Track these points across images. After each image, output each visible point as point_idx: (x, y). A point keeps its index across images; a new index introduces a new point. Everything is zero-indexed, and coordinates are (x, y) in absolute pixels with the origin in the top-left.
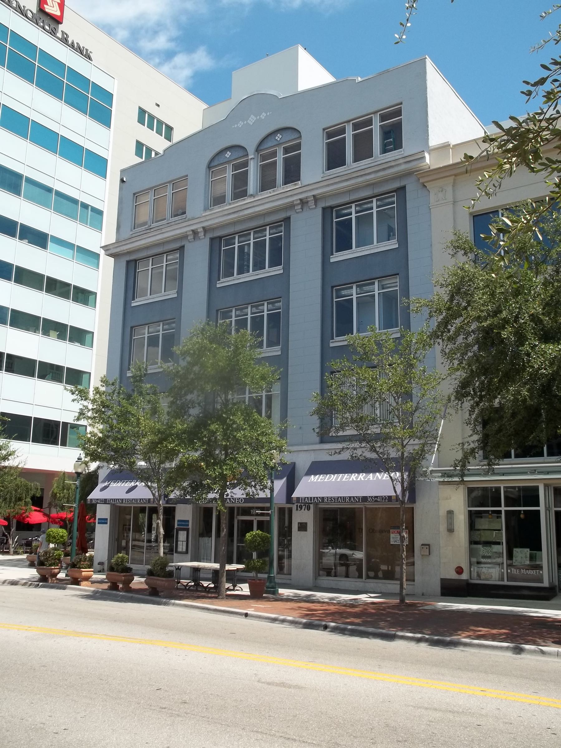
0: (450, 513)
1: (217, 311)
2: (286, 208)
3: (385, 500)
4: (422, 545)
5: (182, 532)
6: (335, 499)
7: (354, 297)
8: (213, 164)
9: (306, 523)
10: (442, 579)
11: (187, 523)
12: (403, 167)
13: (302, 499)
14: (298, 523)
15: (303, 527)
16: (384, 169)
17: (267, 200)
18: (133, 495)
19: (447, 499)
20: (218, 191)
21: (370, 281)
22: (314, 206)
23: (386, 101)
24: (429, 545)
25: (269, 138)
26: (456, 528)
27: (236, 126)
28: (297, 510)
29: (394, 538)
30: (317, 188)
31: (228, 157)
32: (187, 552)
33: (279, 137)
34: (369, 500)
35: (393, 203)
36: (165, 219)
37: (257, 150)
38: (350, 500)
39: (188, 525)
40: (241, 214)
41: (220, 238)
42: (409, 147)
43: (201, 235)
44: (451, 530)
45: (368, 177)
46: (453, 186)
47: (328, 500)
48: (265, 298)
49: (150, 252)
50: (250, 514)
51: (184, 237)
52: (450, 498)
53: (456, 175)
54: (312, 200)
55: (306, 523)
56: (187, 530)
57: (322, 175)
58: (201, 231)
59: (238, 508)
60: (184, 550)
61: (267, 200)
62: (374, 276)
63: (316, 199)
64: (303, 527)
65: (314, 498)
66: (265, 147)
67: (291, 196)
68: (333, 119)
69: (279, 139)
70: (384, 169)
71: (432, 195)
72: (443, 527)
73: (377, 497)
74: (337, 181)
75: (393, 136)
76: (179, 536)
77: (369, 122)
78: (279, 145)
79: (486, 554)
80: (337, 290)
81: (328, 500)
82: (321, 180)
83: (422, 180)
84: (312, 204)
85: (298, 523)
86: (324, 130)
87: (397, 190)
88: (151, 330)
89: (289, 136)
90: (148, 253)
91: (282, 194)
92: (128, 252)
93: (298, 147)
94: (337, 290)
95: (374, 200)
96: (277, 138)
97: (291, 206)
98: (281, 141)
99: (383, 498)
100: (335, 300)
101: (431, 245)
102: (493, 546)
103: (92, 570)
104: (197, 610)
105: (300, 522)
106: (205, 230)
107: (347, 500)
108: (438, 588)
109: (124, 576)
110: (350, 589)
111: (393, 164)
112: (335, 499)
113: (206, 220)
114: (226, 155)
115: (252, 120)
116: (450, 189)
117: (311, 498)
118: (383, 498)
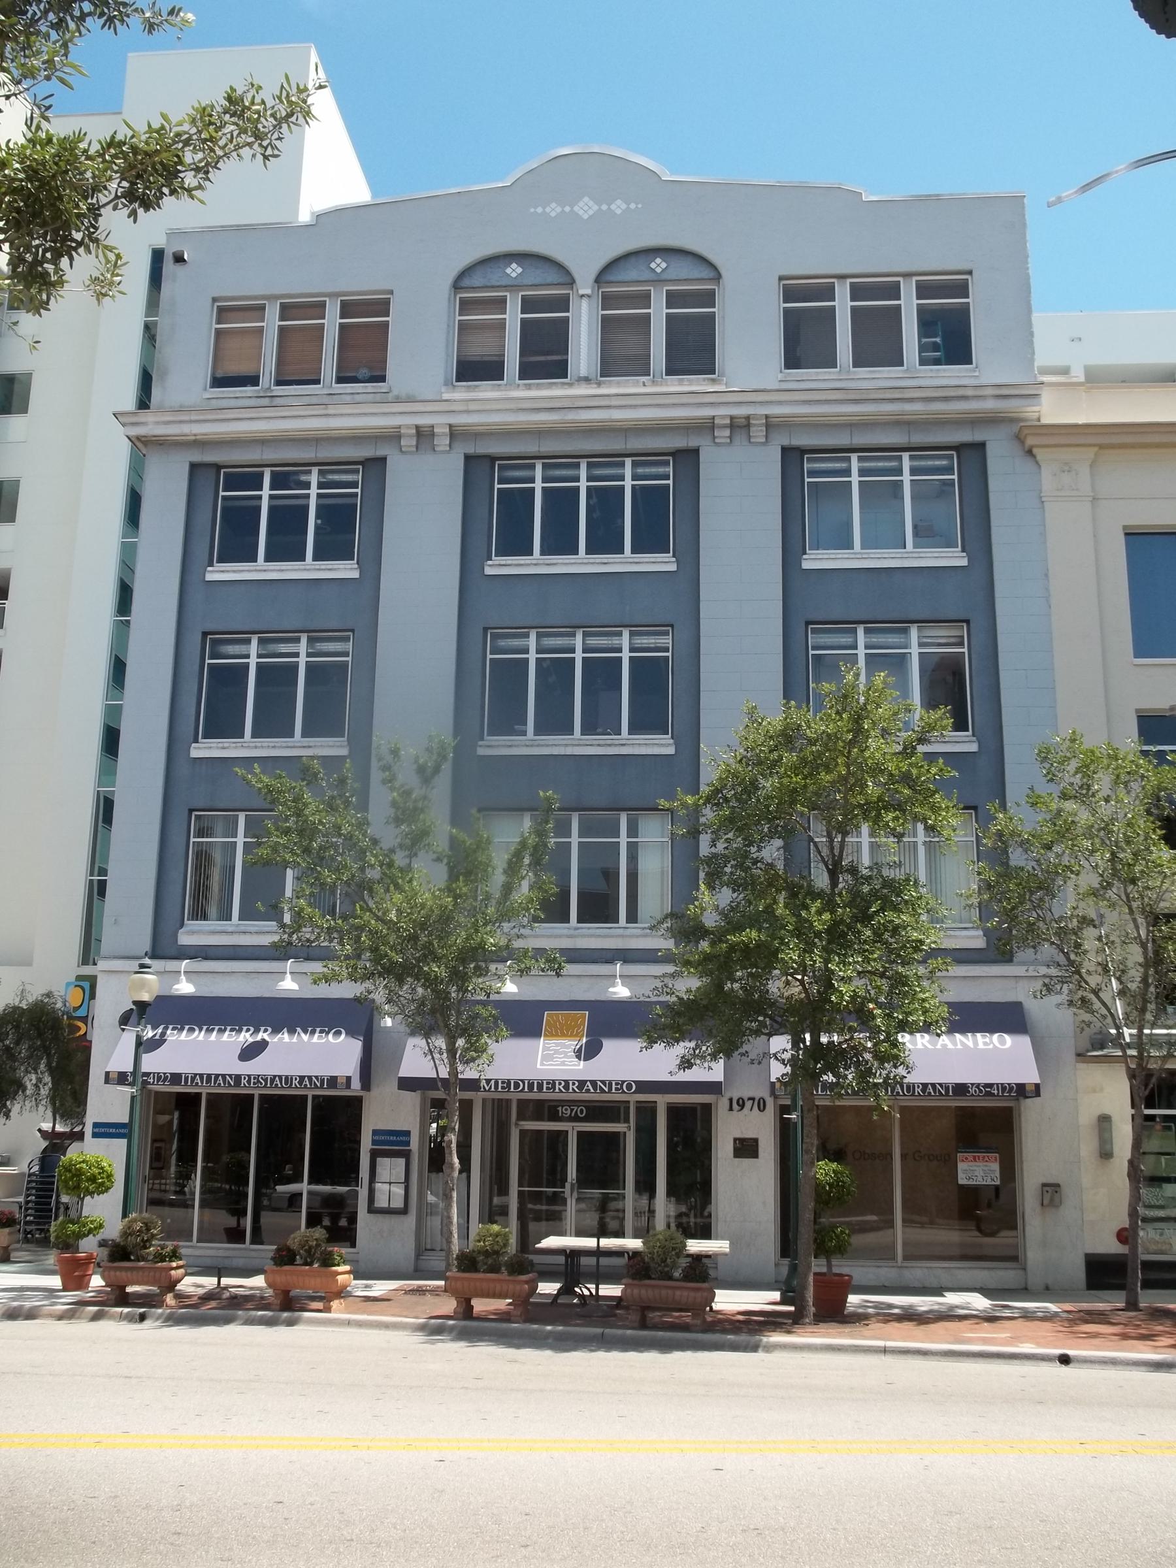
0: (1104, 1121)
1: (485, 629)
2: (376, 437)
3: (165, 1080)
4: (1044, 1185)
5: (996, 1167)
6: (266, 1080)
7: (253, 662)
8: (466, 282)
9: (756, 1141)
10: (1087, 1256)
11: (96, 1130)
12: (990, 405)
13: (186, 1078)
14: (735, 1140)
15: (746, 1148)
16: (946, 399)
17: (647, 401)
18: (258, 1066)
19: (1094, 1091)
20: (480, 349)
21: (901, 625)
22: (763, 440)
23: (361, 281)
24: (1058, 1185)
25: (633, 259)
26: (1116, 1150)
27: (540, 210)
28: (731, 1109)
29: (825, 1170)
30: (780, 403)
31: (514, 275)
32: (404, 1211)
33: (658, 265)
34: (972, 1091)
35: (354, 485)
36: (317, 382)
37: (599, 280)
38: (924, 1090)
39: (408, 1143)
40: (571, 416)
41: (492, 459)
42: (989, 367)
43: (443, 442)
44: (1106, 1154)
45: (908, 407)
46: (1091, 466)
47: (249, 1082)
48: (627, 622)
49: (861, 440)
50: (554, 1116)
51: (393, 437)
52: (1102, 1090)
53: (1101, 447)
54: (760, 425)
55: (756, 1141)
56: (406, 1155)
57: (780, 376)
58: (444, 434)
59: (521, 1102)
60: (398, 1203)
61: (647, 401)
62: (913, 617)
63: (770, 425)
64: (746, 1148)
65: (217, 1076)
66: (620, 278)
67: (712, 404)
68: (810, 262)
69: (659, 270)
70: (946, 399)
71: (1046, 473)
72: (1088, 1148)
73: (990, 1085)
74: (834, 397)
75: (950, 338)
76: (379, 1170)
77: (318, 309)
78: (658, 281)
79: (1154, 1202)
80: (213, 641)
81: (249, 1082)
82: (776, 386)
83: (1030, 441)
84: (758, 433)
85: (735, 1140)
86: (781, 278)
87: (366, 463)
88: (593, 641)
89: (684, 270)
90: (265, 457)
91: (655, 398)
92: (195, 441)
93: (708, 298)
94: (213, 641)
95: (315, 470)
96: (653, 265)
97: (708, 427)
98: (664, 276)
99: (1004, 1089)
100: (208, 661)
101: (1046, 575)
102: (1165, 1186)
103: (181, 1263)
104: (973, 1360)
105: (738, 1136)
106: (455, 434)
107: (918, 1090)
108: (1079, 1273)
109: (527, 1282)
110: (863, 1283)
111: (970, 392)
112: (266, 1080)
113: (468, 412)
114: (508, 271)
115: (586, 208)
116: (1084, 471)
117: (209, 1076)
118: (159, 1078)
